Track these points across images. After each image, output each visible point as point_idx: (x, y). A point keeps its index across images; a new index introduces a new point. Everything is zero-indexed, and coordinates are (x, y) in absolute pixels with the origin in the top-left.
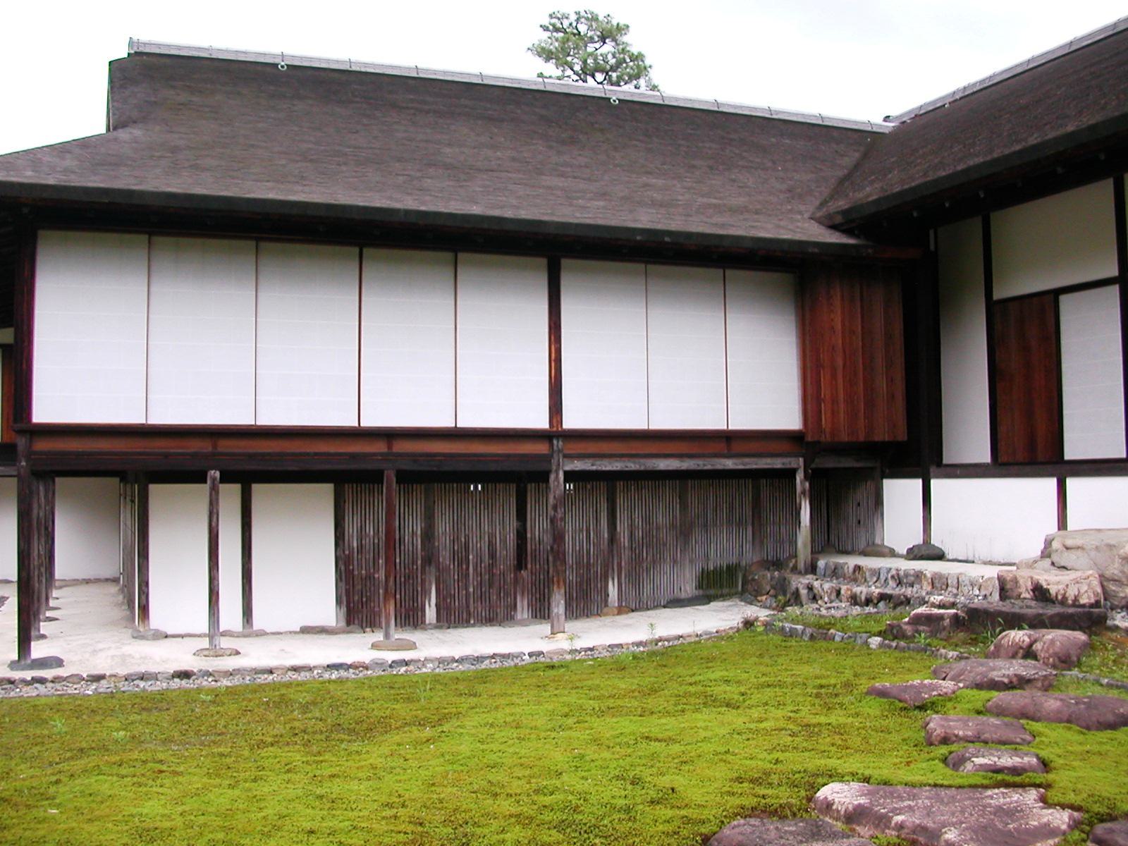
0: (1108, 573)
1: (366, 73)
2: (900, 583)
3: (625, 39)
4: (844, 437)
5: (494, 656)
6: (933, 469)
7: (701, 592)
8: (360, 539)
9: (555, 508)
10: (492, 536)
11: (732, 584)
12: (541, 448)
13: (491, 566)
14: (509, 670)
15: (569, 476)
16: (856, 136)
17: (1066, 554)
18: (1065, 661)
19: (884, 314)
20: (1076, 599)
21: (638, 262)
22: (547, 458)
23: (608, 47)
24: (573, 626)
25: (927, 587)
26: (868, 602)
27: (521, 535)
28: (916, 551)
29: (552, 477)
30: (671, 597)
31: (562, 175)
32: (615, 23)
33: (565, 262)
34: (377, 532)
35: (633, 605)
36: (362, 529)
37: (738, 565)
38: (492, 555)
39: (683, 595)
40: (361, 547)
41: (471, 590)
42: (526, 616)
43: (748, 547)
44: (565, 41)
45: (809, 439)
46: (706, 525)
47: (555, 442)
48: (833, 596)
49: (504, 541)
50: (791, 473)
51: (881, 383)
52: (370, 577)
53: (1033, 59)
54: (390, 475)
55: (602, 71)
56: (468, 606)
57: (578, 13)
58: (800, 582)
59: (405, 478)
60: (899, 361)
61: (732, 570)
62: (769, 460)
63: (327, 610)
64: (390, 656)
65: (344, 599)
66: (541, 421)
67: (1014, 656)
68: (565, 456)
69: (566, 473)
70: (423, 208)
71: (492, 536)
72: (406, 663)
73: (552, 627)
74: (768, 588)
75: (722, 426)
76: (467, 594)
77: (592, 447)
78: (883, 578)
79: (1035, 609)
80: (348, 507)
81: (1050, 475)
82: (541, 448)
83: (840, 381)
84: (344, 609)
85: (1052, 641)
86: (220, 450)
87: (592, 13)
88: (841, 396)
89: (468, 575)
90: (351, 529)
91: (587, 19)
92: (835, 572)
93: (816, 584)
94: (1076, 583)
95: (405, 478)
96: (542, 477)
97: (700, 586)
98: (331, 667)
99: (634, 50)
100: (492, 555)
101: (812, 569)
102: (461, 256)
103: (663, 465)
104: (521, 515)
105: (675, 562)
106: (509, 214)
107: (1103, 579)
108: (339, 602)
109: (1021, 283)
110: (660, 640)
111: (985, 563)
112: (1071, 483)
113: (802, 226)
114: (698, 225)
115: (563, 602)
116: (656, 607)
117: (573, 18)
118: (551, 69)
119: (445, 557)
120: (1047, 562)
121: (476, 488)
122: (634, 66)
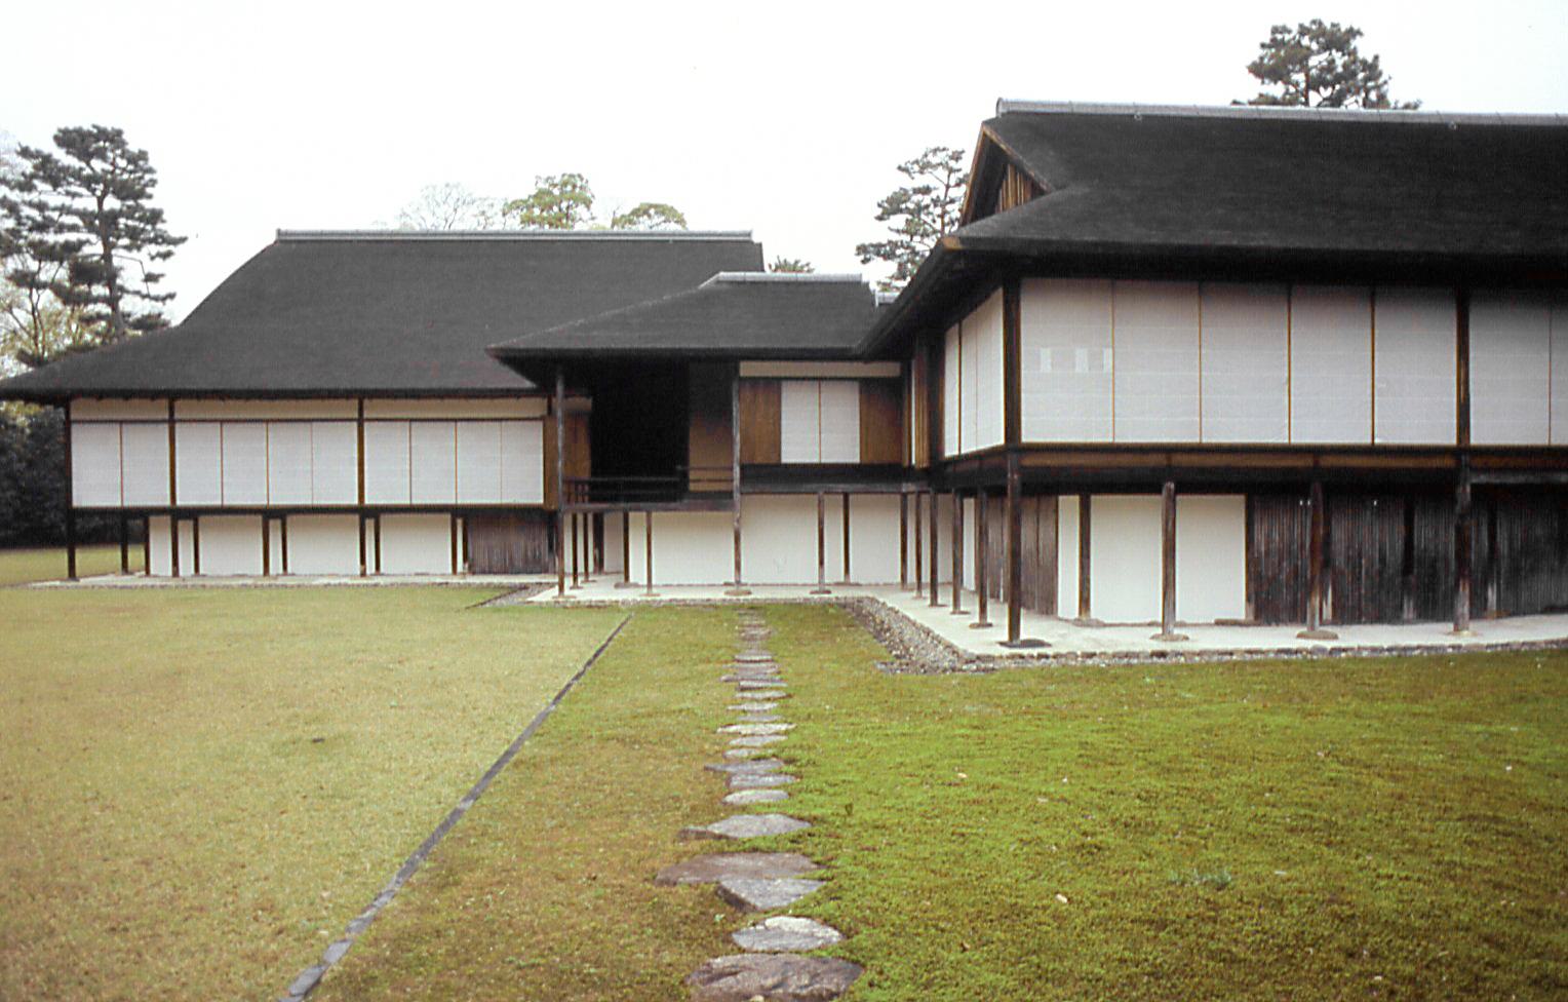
1: (1037, 114)
8: (1268, 544)
12: (1448, 462)
13: (1381, 573)
16: (758, 263)
24: (1474, 625)
34: (1281, 536)
35: (1512, 608)
36: (1269, 536)
38: (1382, 560)
40: (1267, 553)
41: (1363, 591)
42: (1411, 616)
47: (1463, 458)
49: (1392, 547)
52: (1275, 578)
56: (1360, 604)
63: (1239, 609)
64: (1309, 644)
65: (1253, 597)
66: (1451, 440)
69: (1473, 486)
76: (1360, 595)
80: (1257, 517)
84: (1253, 606)
89: (1359, 579)
90: (1260, 538)
100: (1382, 560)
105: (1552, 571)
108: (1248, 599)
115: (1467, 603)
117: (1295, 29)
119: (1340, 561)
121: (1305, 502)
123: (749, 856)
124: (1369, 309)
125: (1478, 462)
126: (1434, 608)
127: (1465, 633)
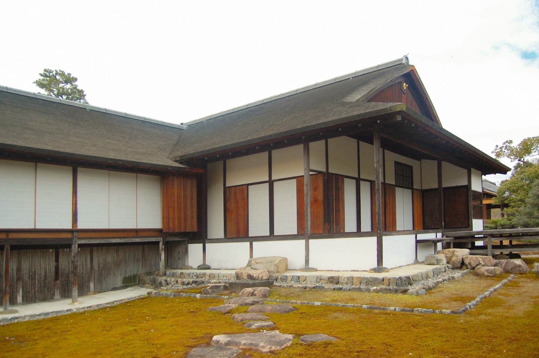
0: (270, 270)
2: (197, 277)
3: (76, 83)
4: (177, 231)
5: (53, 312)
6: (206, 241)
7: (123, 285)
9: (74, 257)
10: (45, 269)
11: (135, 281)
12: (69, 236)
13: (45, 280)
14: (84, 314)
15: (80, 246)
17: (256, 265)
18: (265, 296)
19: (190, 189)
20: (262, 278)
21: (32, 162)
22: (71, 239)
23: (68, 86)
24: (80, 299)
25: (207, 278)
26: (188, 284)
27: (57, 268)
28: (201, 267)
29: (73, 246)
30: (113, 287)
31: (78, 137)
32: (72, 76)
33: (79, 169)
35: (100, 290)
37: (137, 275)
39: (117, 286)
41: (37, 289)
42: (58, 297)
43: (140, 268)
44: (49, 79)
45: (165, 231)
46: (126, 261)
48: (175, 283)
50: (158, 243)
51: (189, 213)
53: (235, 109)
54: (7, 247)
55: (65, 94)
56: (35, 295)
57: (56, 71)
58: (162, 279)
59: (14, 248)
60: (195, 206)
61: (135, 276)
62: (151, 239)
66: (69, 226)
67: (248, 296)
68: (78, 238)
70: (27, 146)
71: (45, 269)
72: (17, 318)
73: (73, 300)
74: (148, 282)
75: (135, 227)
77: (88, 235)
78: (191, 276)
79: (251, 282)
81: (248, 241)
82: (69, 236)
83: (176, 212)
85: (260, 290)
86: (9, 237)
87: (63, 72)
88: (176, 217)
89: (35, 284)
91: (60, 74)
92: (173, 275)
93: (168, 279)
94: (260, 273)
95: (14, 248)
96: (69, 246)
97: (123, 283)
98: (67, 311)
99: (79, 88)
101: (165, 274)
102: (38, 164)
103: (114, 241)
104: (57, 260)
106: (61, 150)
107: (269, 272)
109: (234, 181)
110: (115, 301)
111: (225, 269)
112: (255, 244)
113: (165, 160)
114: (123, 157)
115: (77, 291)
116: (108, 291)
117: (54, 73)
118: (43, 92)
119: (26, 277)
120: (250, 268)
122: (81, 94)
123: (257, 334)
124: (34, 174)
125: (82, 235)
126: (66, 294)
127: (76, 303)
